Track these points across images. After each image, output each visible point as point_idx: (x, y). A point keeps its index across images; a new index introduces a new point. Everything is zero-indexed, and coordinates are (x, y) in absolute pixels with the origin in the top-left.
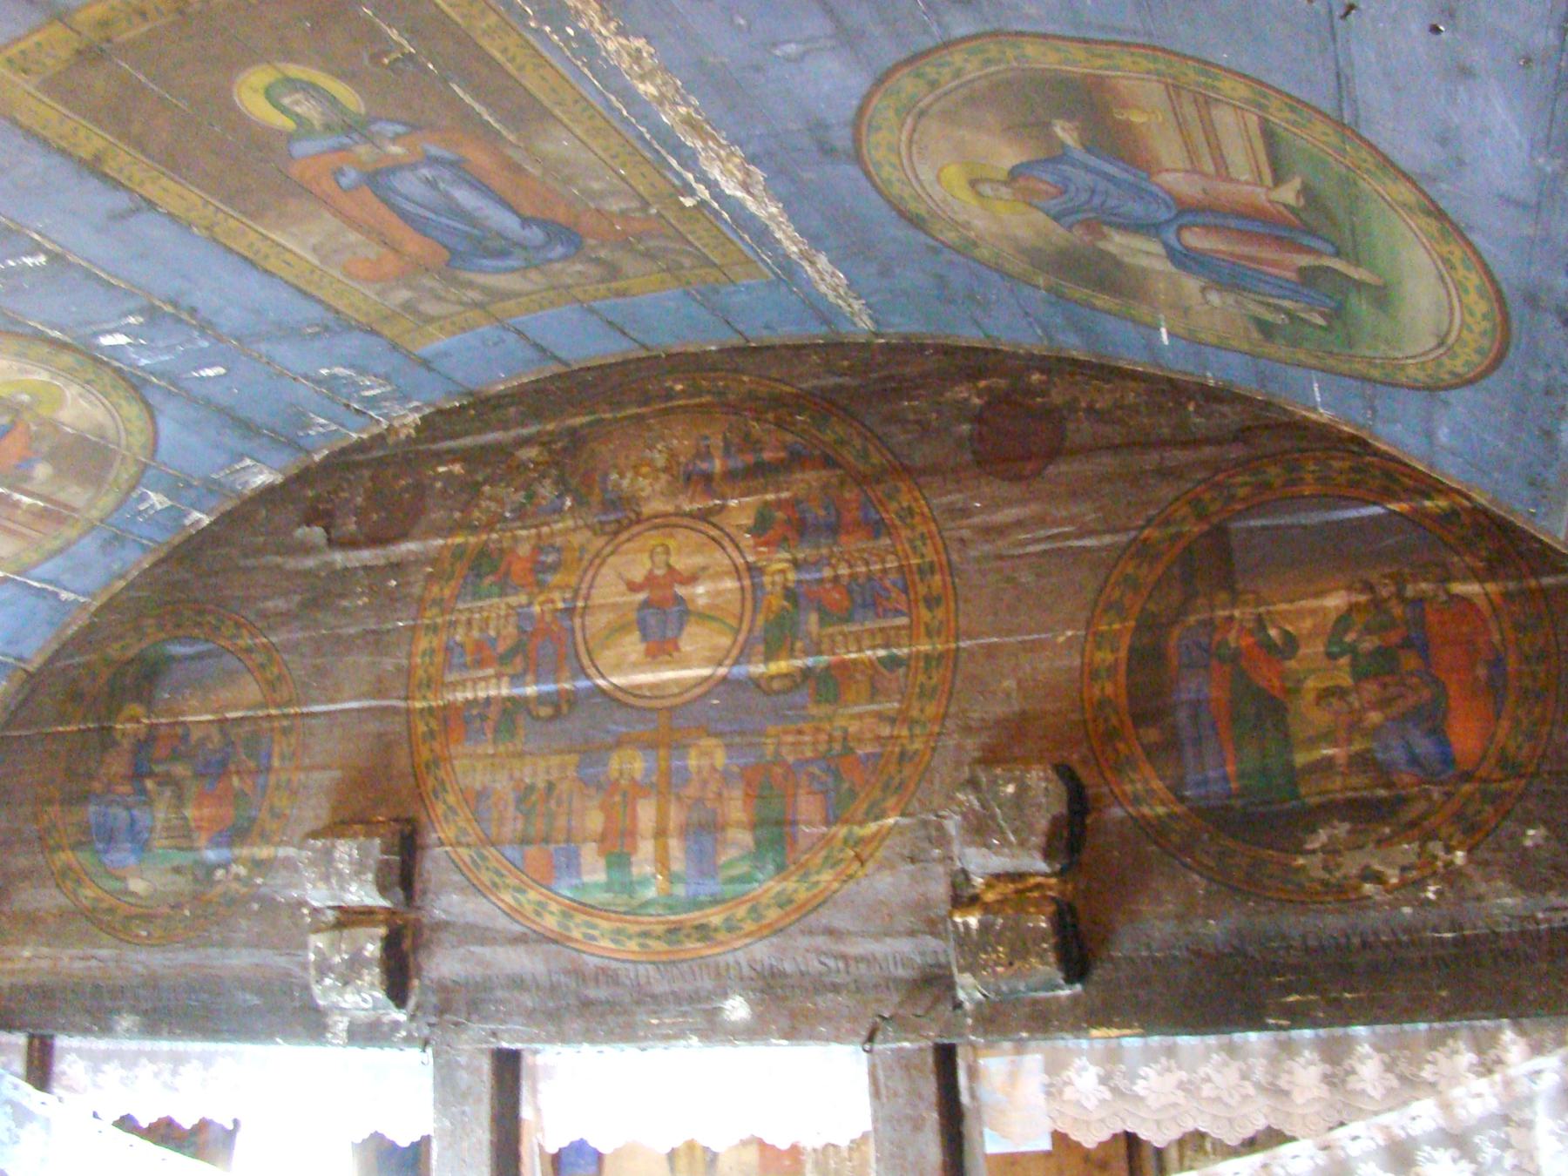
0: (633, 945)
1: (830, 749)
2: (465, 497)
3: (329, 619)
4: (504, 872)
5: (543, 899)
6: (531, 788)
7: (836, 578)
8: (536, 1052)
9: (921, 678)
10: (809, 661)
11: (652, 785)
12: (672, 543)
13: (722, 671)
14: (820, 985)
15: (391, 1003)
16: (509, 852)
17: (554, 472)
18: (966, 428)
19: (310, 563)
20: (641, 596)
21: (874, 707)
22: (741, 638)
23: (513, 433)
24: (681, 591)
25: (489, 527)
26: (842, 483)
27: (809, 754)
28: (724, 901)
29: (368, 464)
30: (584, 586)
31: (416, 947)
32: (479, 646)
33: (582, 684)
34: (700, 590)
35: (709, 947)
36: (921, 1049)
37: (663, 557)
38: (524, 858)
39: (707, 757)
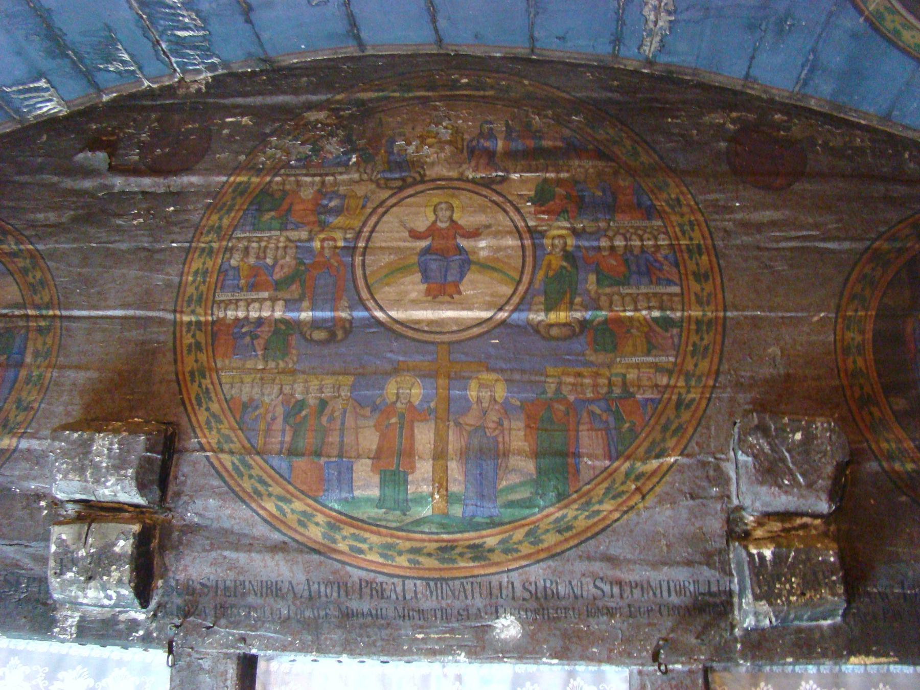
0: (403, 561)
1: (610, 392)
2: (250, 144)
3: (103, 235)
4: (270, 481)
5: (309, 510)
6: (301, 405)
7: (612, 248)
8: (269, 659)
9: (694, 338)
10: (588, 315)
11: (430, 411)
12: (455, 203)
13: (502, 315)
14: (593, 609)
15: (136, 602)
16: (275, 462)
17: (341, 133)
18: (723, 145)
19: (88, 184)
20: (424, 244)
21: (650, 359)
22: (522, 289)
23: (303, 98)
24: (463, 243)
25: (275, 170)
26: (616, 173)
27: (589, 395)
28: (501, 524)
29: (153, 108)
30: (367, 229)
31: (162, 548)
32: (254, 271)
33: (360, 314)
34: (483, 244)
35: (483, 567)
36: (690, 672)
37: (448, 213)
38: (291, 468)
39: (486, 390)
